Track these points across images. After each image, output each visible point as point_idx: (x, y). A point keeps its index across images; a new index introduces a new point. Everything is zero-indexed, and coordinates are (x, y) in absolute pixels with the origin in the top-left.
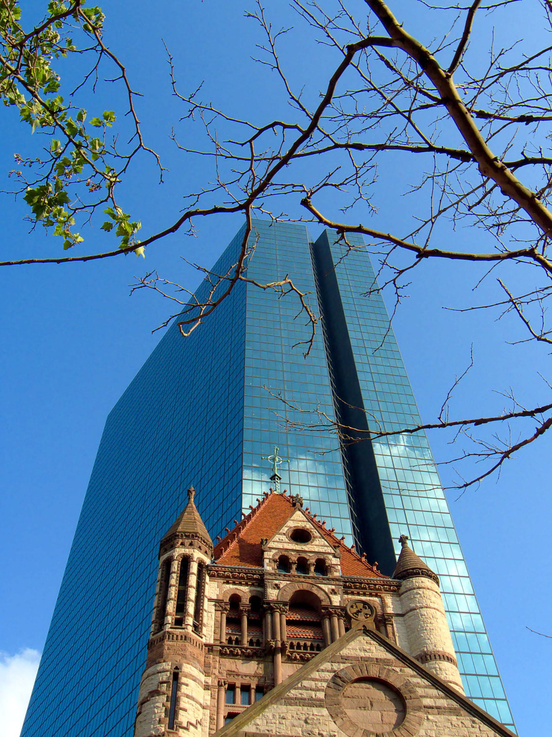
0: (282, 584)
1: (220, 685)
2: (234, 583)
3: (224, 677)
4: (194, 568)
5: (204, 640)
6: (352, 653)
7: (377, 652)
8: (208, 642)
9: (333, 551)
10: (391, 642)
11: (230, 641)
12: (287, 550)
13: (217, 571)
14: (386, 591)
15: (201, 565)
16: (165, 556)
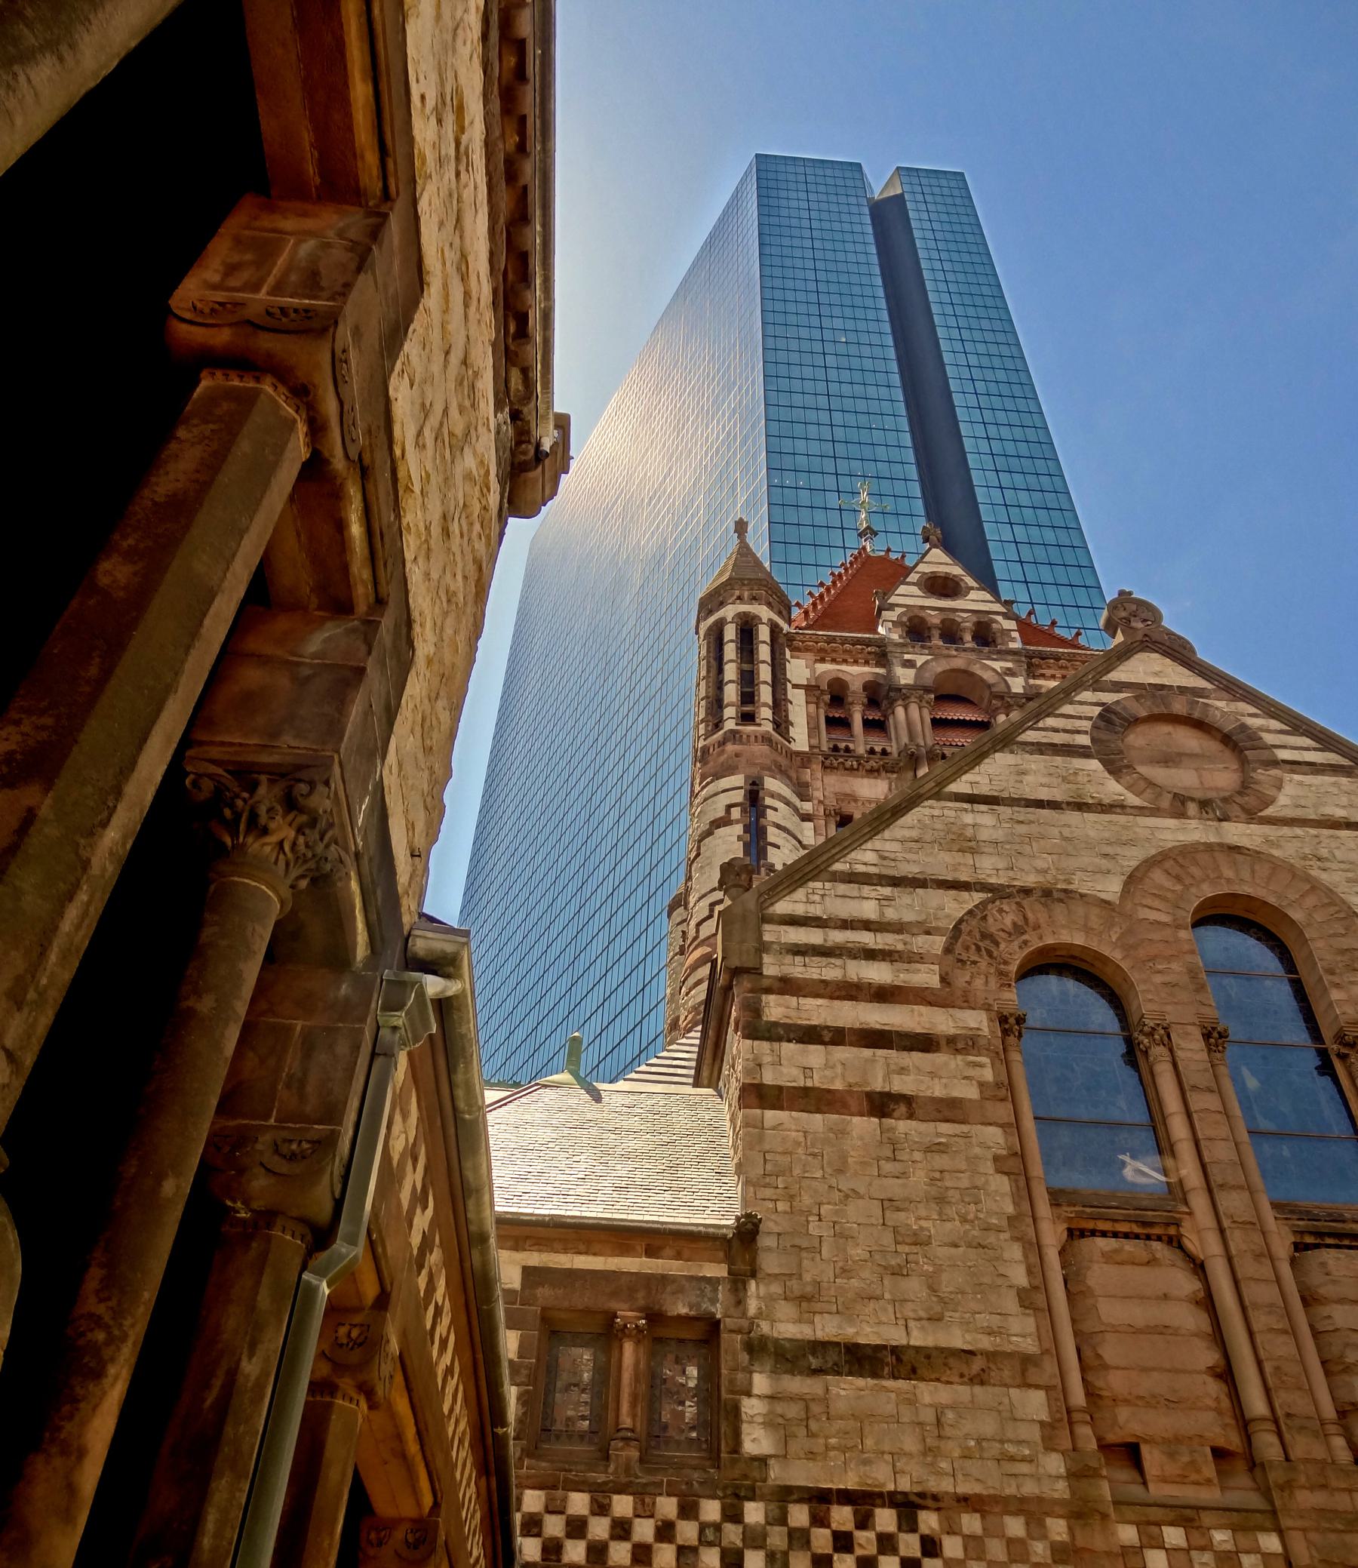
0: (920, 660)
1: (827, 815)
2: (834, 661)
3: (831, 802)
4: (764, 633)
12: (922, 608)
15: (774, 629)
16: (712, 619)
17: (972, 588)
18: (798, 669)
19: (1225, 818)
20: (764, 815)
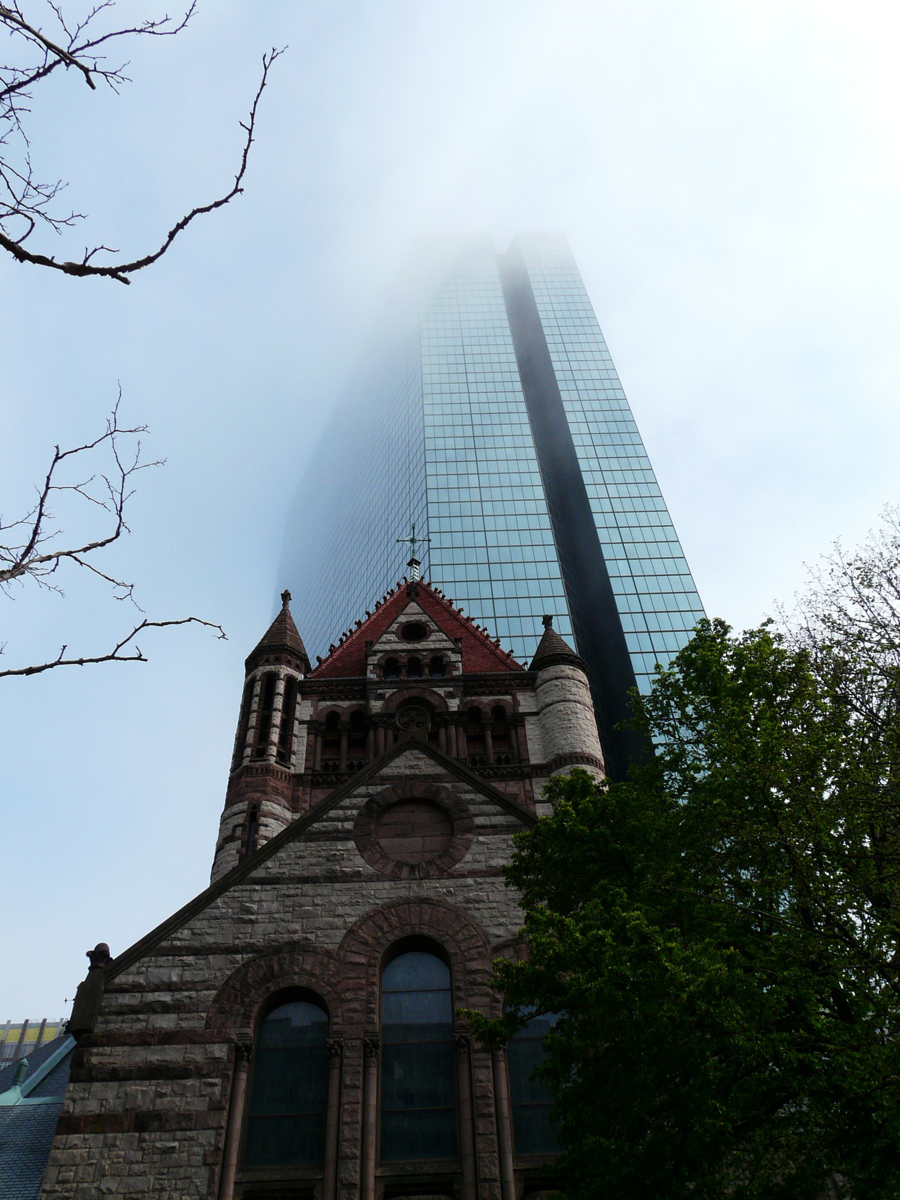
0: (389, 693)
2: (331, 699)
4: (281, 687)
5: (292, 770)
6: (396, 772)
7: (426, 766)
8: (298, 772)
9: (453, 646)
10: (442, 752)
11: (325, 767)
12: (396, 651)
13: (310, 687)
14: (518, 686)
17: (434, 631)
18: (304, 710)
19: (428, 877)
20: (257, 832)
